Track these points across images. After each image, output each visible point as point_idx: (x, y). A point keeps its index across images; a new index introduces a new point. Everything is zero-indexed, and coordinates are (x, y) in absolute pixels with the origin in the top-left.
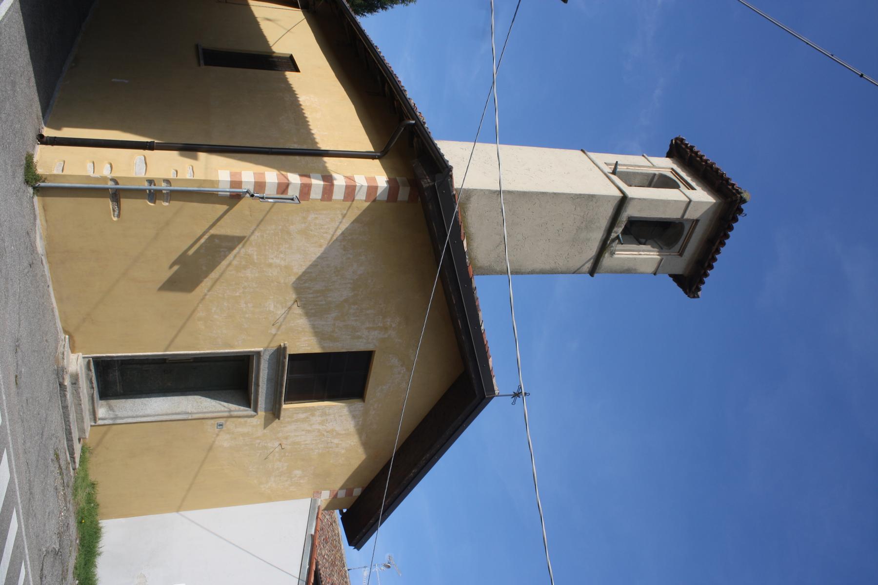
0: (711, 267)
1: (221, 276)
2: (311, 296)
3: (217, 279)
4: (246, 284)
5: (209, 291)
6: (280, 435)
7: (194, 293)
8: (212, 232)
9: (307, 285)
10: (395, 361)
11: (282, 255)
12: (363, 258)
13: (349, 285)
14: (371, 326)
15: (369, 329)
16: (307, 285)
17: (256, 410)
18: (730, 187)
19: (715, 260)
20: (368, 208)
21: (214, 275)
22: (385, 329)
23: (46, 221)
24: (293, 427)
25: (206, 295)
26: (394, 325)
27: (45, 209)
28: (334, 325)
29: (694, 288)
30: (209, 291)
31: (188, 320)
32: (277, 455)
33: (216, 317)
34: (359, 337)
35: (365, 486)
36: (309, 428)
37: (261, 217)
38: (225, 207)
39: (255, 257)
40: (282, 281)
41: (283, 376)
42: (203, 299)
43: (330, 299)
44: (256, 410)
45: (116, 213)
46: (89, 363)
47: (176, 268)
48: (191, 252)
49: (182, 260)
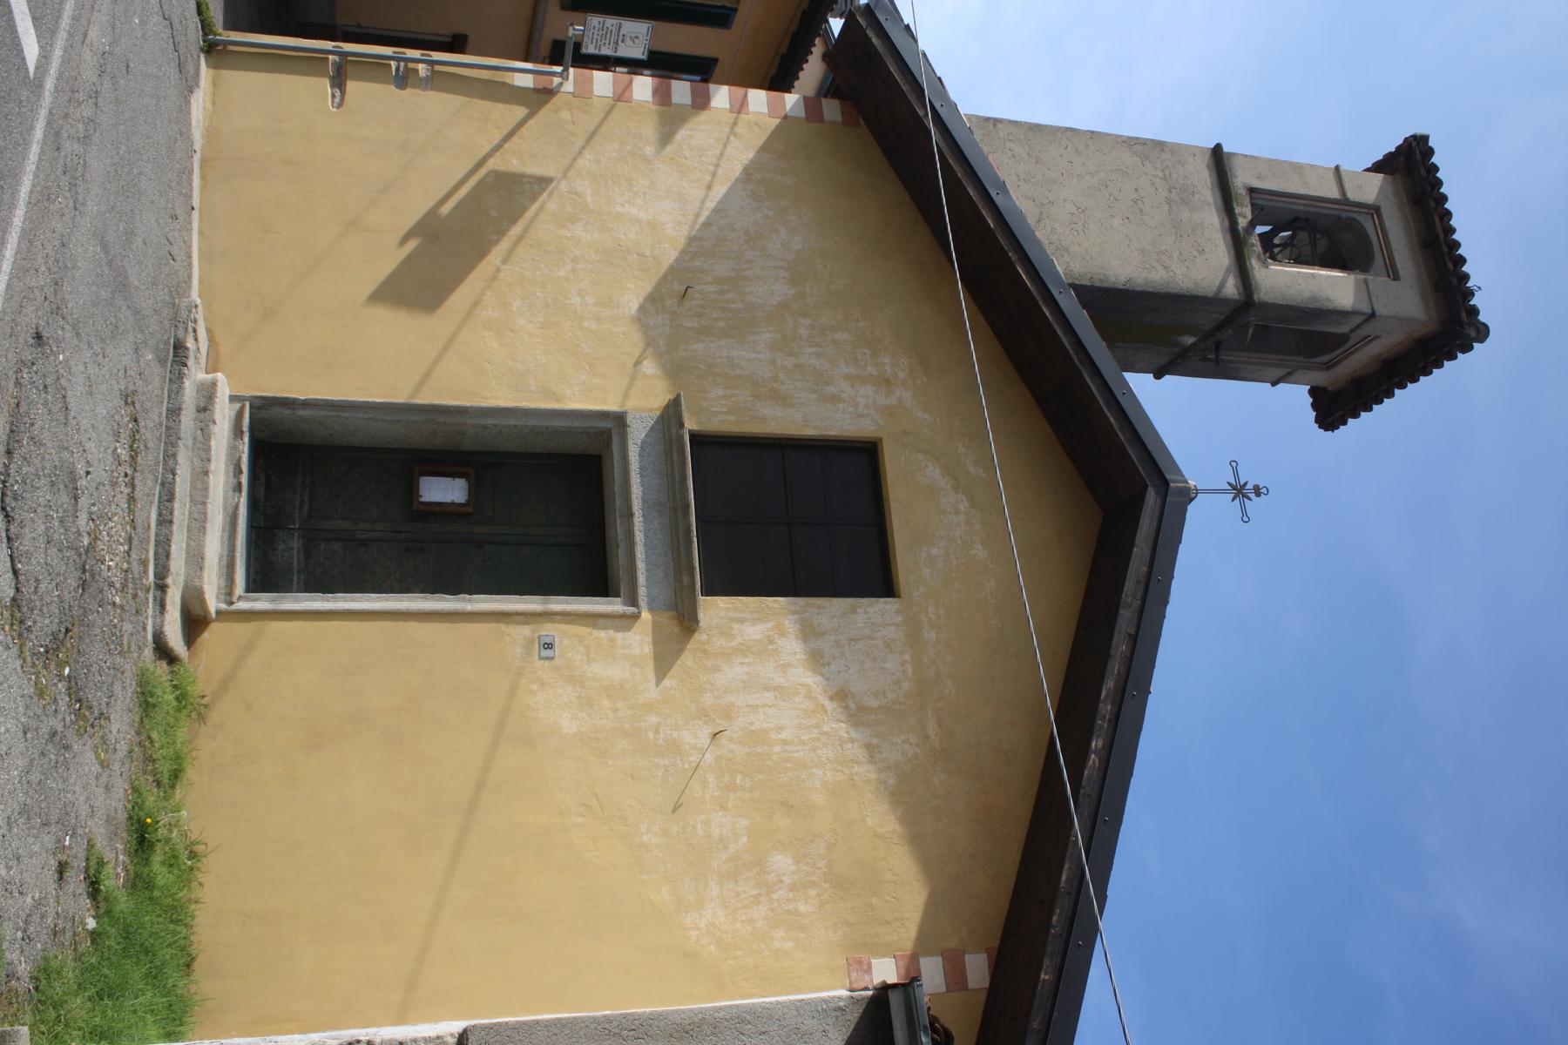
0: (1463, 261)
1: (526, 230)
2: (711, 288)
3: (520, 239)
4: (577, 252)
5: (504, 262)
6: (708, 699)
7: (440, 312)
8: (492, 164)
9: (697, 263)
10: (934, 473)
11: (639, 201)
12: (794, 218)
13: (782, 273)
14: (853, 371)
15: (846, 377)
16: (697, 263)
17: (633, 601)
18: (1454, 281)
19: (1457, 245)
20: (778, 128)
21: (515, 230)
22: (886, 382)
23: (214, 103)
24: (733, 672)
25: (498, 270)
26: (901, 375)
27: (215, 84)
28: (773, 362)
29: (1464, 315)
30: (504, 262)
31: (463, 323)
32: (711, 778)
33: (521, 322)
34: (835, 399)
35: (995, 943)
36: (779, 680)
37: (592, 128)
38: (520, 112)
39: (589, 199)
40: (648, 253)
41: (684, 478)
42: (494, 279)
43: (751, 298)
44: (633, 601)
45: (337, 100)
46: (240, 414)
47: (412, 245)
48: (446, 209)
49: (429, 229)
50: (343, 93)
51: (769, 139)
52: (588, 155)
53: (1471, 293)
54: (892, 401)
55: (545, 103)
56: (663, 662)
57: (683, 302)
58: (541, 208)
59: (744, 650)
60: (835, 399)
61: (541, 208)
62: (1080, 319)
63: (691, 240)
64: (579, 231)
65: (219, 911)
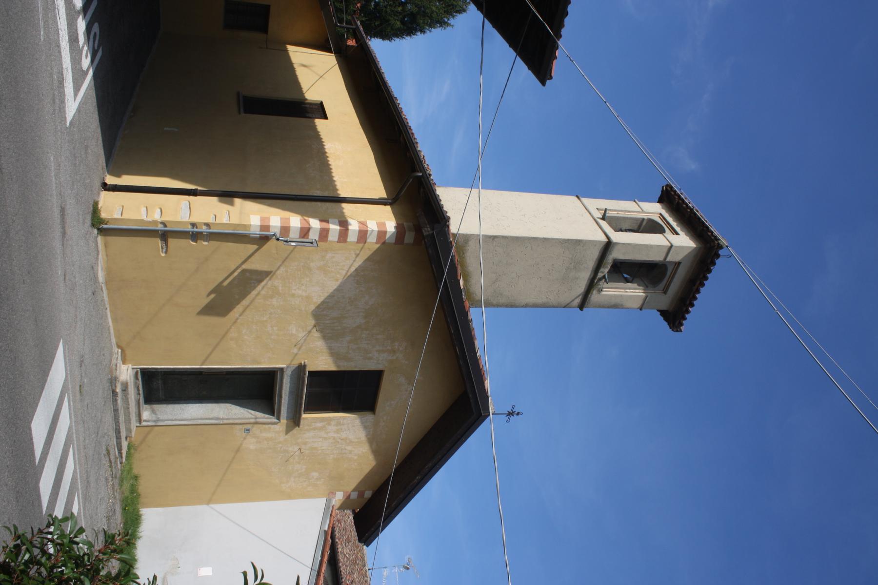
6: (300, 440)
11: (303, 288)
17: (278, 418)
21: (245, 302)
23: (107, 255)
35: (376, 489)
38: (252, 247)
42: (235, 322)
44: (278, 418)
46: (137, 373)
47: (212, 296)
48: (225, 284)
49: (218, 290)
50: (167, 245)
51: (372, 254)
52: (282, 269)
53: (693, 305)
54: (394, 358)
55: (265, 244)
56: (288, 430)
57: (327, 318)
58: (266, 284)
59: (314, 429)
60: (370, 358)
61: (258, 294)
62: (678, 229)
63: (323, 302)
64: (274, 302)
65: (143, 487)
